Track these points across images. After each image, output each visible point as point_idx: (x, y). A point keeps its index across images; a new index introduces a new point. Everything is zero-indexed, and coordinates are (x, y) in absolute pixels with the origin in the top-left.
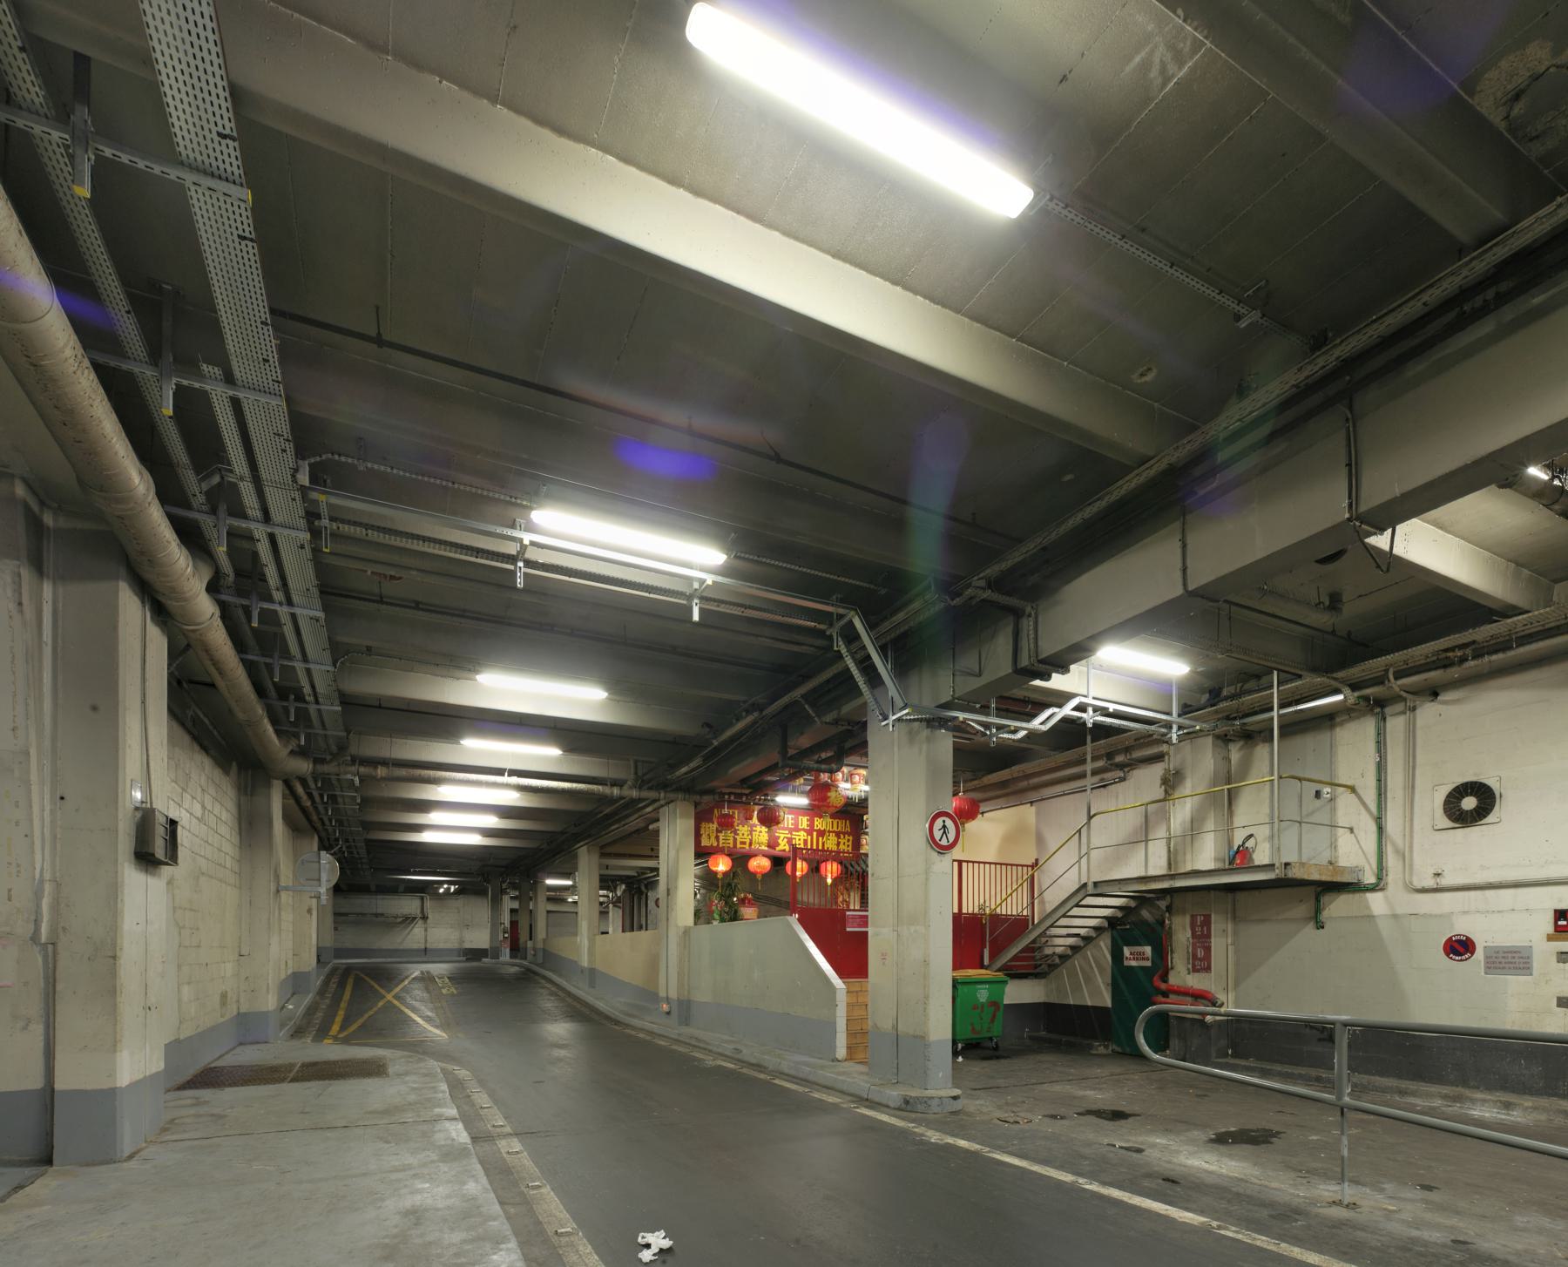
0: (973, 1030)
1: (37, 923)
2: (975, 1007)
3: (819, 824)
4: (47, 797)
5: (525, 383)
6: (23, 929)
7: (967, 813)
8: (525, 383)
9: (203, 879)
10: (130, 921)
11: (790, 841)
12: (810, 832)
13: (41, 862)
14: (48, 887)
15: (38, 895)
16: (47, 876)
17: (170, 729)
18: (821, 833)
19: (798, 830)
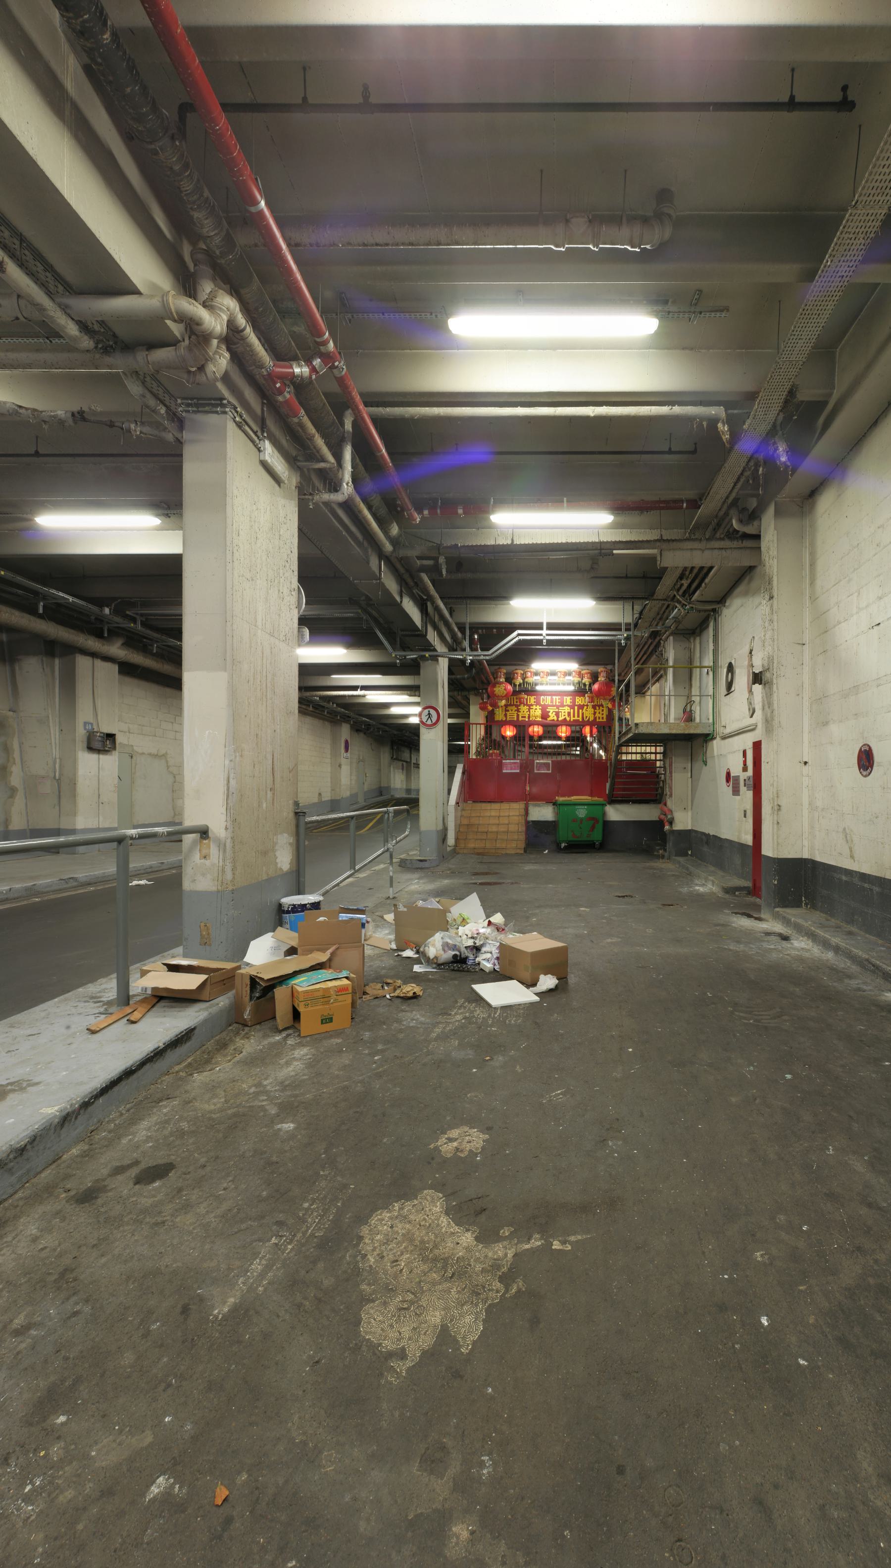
0: (574, 835)
1: (55, 773)
2: (574, 821)
3: (579, 700)
4: (57, 730)
5: (163, 455)
6: (52, 775)
7: (761, 672)
8: (163, 455)
9: (592, 822)
10: (82, 771)
11: (557, 714)
12: (572, 707)
13: (56, 753)
14: (58, 761)
15: (55, 763)
16: (58, 756)
17: (746, 594)
18: (581, 707)
19: (564, 706)
